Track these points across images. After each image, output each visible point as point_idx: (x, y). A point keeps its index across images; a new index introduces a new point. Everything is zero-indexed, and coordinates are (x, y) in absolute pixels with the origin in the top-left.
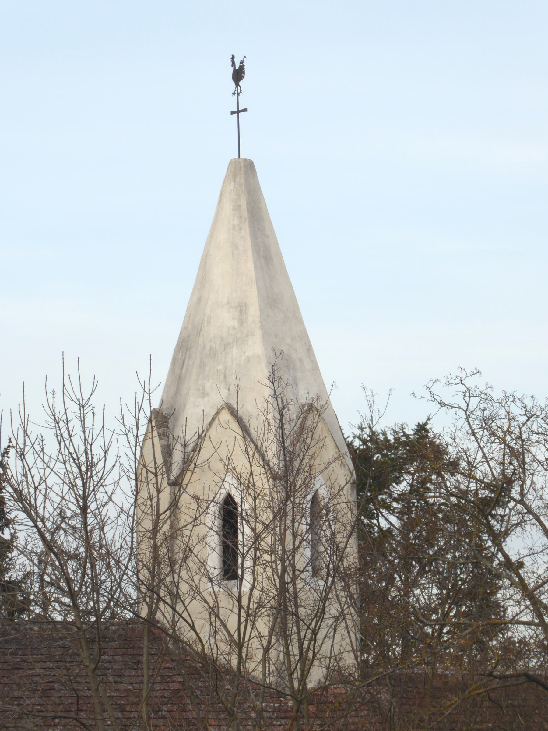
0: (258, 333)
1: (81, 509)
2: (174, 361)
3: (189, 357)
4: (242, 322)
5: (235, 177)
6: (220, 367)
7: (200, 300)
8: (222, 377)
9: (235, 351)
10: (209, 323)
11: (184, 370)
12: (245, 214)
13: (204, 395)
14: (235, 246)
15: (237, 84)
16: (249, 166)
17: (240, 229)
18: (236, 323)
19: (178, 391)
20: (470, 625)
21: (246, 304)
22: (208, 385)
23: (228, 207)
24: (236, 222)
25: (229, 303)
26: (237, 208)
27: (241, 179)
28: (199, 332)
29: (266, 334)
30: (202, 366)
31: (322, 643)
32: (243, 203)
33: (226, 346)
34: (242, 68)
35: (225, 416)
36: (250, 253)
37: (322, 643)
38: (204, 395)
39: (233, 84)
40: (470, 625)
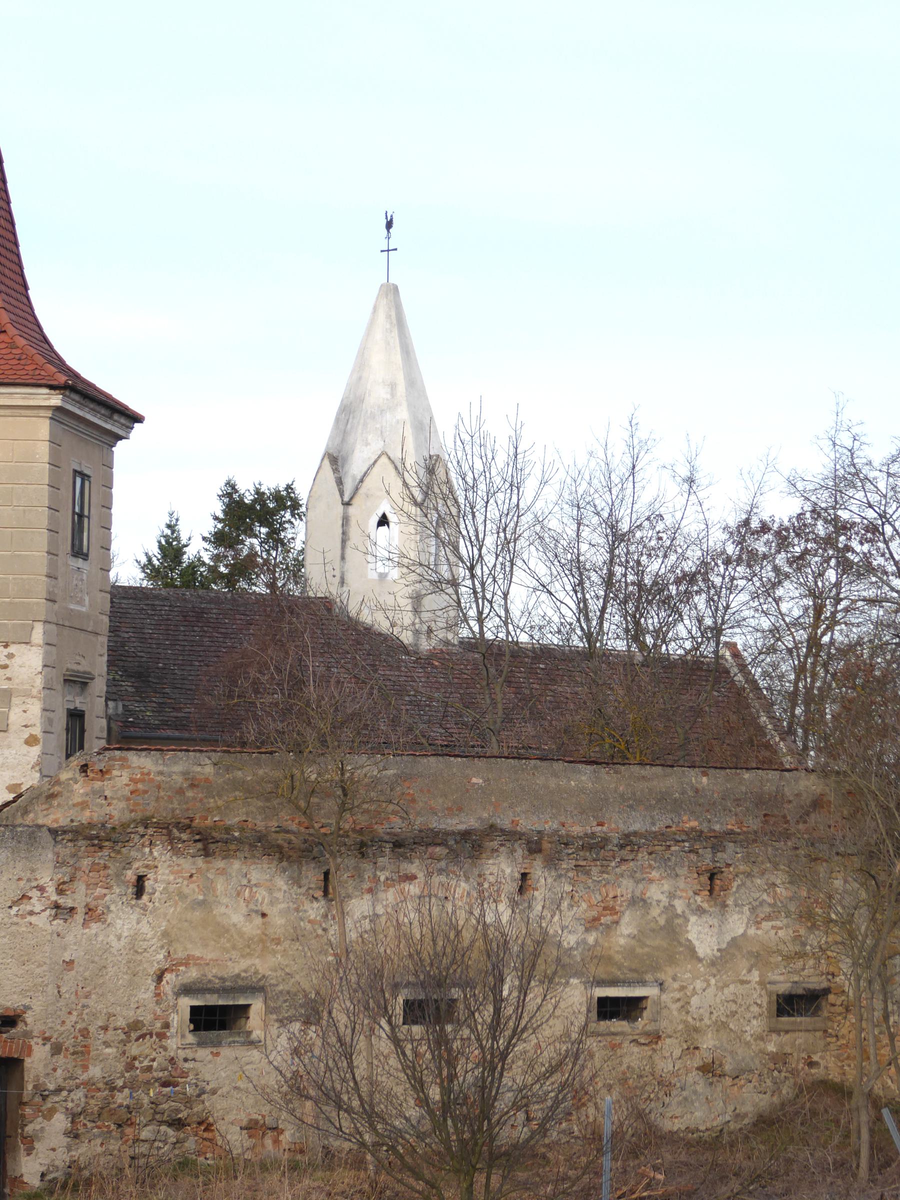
0: (405, 404)
1: (550, 1065)
2: (337, 420)
3: (353, 418)
4: (393, 395)
5: (387, 295)
6: (378, 426)
7: (360, 378)
8: (379, 432)
9: (388, 415)
10: (370, 395)
11: (349, 426)
12: (395, 322)
13: (367, 444)
14: (388, 343)
15: (388, 231)
16: (396, 289)
17: (391, 331)
18: (389, 396)
19: (343, 440)
20: (372, 688)
21: (395, 384)
22: (370, 437)
23: (378, 335)
24: (388, 326)
25: (383, 382)
26: (389, 317)
27: (391, 296)
28: (362, 401)
29: (409, 405)
30: (365, 425)
31: (519, 500)
32: (393, 314)
33: (382, 411)
34: (392, 220)
35: (384, 459)
36: (398, 349)
37: (519, 500)
38: (367, 444)
39: (386, 231)
40: (372, 688)
